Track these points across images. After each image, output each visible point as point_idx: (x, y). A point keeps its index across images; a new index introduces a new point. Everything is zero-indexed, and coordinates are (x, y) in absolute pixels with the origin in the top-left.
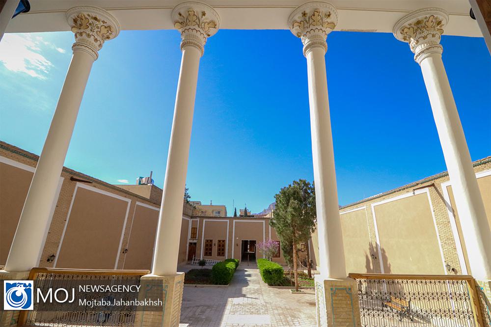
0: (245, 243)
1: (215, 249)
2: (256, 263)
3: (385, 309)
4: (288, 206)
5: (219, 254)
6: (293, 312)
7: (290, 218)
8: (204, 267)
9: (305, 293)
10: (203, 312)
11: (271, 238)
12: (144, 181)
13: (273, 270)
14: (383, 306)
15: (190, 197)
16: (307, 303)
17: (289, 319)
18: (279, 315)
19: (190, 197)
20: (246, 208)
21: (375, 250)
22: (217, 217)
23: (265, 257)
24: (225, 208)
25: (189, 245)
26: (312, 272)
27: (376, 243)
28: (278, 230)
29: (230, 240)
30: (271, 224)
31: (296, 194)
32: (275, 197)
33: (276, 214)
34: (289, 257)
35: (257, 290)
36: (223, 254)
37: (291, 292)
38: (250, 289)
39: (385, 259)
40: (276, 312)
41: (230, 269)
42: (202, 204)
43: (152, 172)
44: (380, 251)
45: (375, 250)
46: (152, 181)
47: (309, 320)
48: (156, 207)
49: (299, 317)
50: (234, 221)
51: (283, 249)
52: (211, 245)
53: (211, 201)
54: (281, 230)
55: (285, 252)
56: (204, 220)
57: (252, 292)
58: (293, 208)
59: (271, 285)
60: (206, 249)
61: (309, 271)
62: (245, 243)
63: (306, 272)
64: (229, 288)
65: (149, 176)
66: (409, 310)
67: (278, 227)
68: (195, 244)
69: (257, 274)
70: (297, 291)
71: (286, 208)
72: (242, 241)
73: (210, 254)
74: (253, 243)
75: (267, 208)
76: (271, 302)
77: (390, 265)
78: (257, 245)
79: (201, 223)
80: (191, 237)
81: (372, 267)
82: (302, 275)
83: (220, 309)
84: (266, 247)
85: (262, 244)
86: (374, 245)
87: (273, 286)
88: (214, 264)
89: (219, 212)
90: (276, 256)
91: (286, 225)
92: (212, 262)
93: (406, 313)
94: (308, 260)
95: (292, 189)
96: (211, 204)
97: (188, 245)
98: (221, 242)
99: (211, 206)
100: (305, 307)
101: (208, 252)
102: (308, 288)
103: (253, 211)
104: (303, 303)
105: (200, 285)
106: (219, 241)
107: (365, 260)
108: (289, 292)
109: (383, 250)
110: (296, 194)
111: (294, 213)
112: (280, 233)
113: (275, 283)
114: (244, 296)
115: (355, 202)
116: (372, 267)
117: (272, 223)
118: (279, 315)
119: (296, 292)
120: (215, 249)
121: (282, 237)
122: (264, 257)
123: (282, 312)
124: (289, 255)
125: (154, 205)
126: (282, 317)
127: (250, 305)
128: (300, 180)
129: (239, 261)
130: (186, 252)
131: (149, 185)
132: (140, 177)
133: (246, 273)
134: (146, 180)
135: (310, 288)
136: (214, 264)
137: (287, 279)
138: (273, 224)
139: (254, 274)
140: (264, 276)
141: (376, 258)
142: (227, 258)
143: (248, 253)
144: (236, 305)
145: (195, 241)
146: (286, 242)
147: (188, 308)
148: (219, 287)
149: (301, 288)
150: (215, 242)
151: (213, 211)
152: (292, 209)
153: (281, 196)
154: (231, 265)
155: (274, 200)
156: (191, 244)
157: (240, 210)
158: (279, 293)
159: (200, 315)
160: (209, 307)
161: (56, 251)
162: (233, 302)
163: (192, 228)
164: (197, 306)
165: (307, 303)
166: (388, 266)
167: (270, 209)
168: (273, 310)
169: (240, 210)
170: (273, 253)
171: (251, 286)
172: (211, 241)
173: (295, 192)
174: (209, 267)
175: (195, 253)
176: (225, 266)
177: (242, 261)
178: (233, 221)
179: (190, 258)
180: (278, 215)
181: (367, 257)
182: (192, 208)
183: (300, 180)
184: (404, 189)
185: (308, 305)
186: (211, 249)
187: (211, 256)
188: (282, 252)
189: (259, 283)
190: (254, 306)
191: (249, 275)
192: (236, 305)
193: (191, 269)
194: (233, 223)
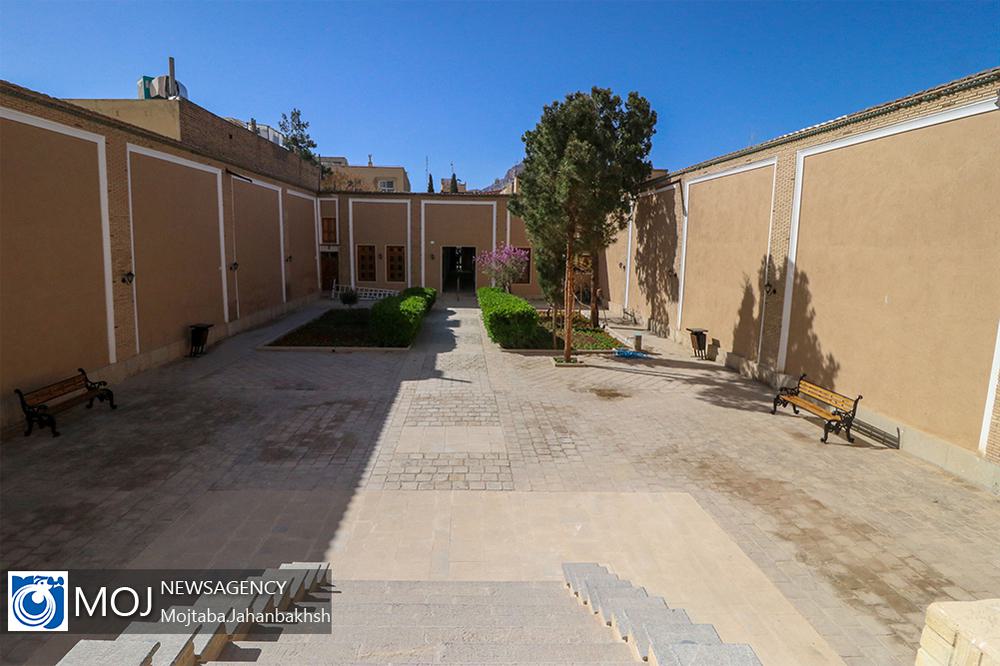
0: (450, 254)
1: (382, 267)
2: (475, 295)
3: (780, 408)
4: (561, 155)
5: (392, 277)
6: (560, 418)
7: (564, 191)
8: (354, 307)
9: (587, 366)
10: (340, 419)
11: (511, 243)
12: (156, 87)
13: (513, 316)
14: (777, 401)
15: (314, 146)
16: (592, 390)
17: (551, 436)
18: (527, 425)
19: (314, 146)
20: (454, 176)
21: (778, 276)
22: (370, 193)
23: (496, 285)
24: (405, 174)
25: (322, 259)
26: (601, 313)
27: (786, 259)
28: (531, 222)
29: (416, 247)
30: (513, 207)
31: (587, 122)
32: (524, 140)
33: (527, 182)
34: (554, 287)
35: (476, 358)
36: (402, 277)
37: (554, 363)
38: (459, 356)
39: (802, 296)
40: (519, 416)
41: (410, 313)
42: (350, 164)
43: (172, 60)
44: (790, 276)
45: (778, 276)
46: (178, 88)
47: (600, 438)
48: (201, 162)
49: (576, 430)
50: (423, 202)
51: (539, 269)
52: (372, 258)
53: (370, 156)
54: (540, 223)
55: (545, 276)
56: (351, 201)
57: (463, 364)
58: (575, 164)
59: (506, 346)
60: (391, 268)
61: (593, 313)
62: (450, 254)
63: (587, 314)
64: (413, 356)
65: (168, 75)
66: (848, 420)
67: (533, 216)
68: (335, 254)
69: (477, 320)
70: (568, 360)
71: (554, 164)
72: (444, 248)
73: (372, 277)
74: (469, 252)
75: (502, 177)
76: (508, 389)
77: (813, 312)
78: (477, 259)
79: (344, 206)
80: (324, 241)
81: (756, 314)
82: (578, 321)
83: (377, 411)
84: (499, 262)
85: (491, 256)
86: (778, 263)
87: (512, 348)
88: (382, 297)
89: (392, 184)
90: (521, 281)
91: (552, 209)
92: (370, 296)
93: (843, 425)
94: (595, 291)
95: (574, 107)
96: (370, 163)
97: (318, 257)
98: (396, 250)
99: (371, 167)
100: (587, 402)
101: (367, 272)
102: (591, 353)
103: (474, 182)
104: (582, 390)
105: (341, 348)
106: (391, 249)
107: (741, 296)
108: (550, 363)
109: (802, 279)
110: (587, 122)
111: (576, 177)
112: (537, 231)
113: (516, 343)
114: (439, 375)
115: (702, 161)
116: (756, 314)
117: (516, 204)
118: (527, 425)
119: (564, 363)
120: (382, 267)
121: (540, 241)
122: (494, 285)
123: (532, 416)
124: (554, 283)
125: (195, 155)
126: (534, 431)
127: (457, 398)
128: (595, 91)
129: (435, 293)
130: (316, 273)
131: (171, 98)
132: (145, 78)
133: (451, 318)
134: (160, 82)
135: (597, 353)
136: (382, 297)
137: (543, 331)
138: (517, 208)
139: (469, 322)
140: (491, 328)
141: (775, 292)
142: (409, 286)
143: (460, 273)
144: (424, 399)
145: (334, 249)
146: (550, 253)
147: (305, 408)
148: (387, 352)
149: (577, 354)
150: (381, 249)
151: (376, 181)
152: (573, 166)
153: (544, 131)
154: (413, 305)
155: (520, 155)
156: (324, 255)
157: (443, 180)
158: (526, 367)
159: (331, 428)
160: (356, 404)
161: (131, 267)
162: (411, 392)
163: (323, 219)
164: (328, 404)
165: (592, 390)
166: (808, 315)
167: (508, 177)
168: (512, 411)
169: (443, 180)
170: (514, 276)
171: (463, 349)
172: (372, 248)
173: (584, 116)
174: (365, 303)
175: (336, 274)
176: (398, 308)
177: (443, 290)
178: (420, 203)
179: (327, 286)
180: (532, 183)
181: (748, 292)
182: (318, 172)
183: (595, 91)
184: (939, 96)
185: (595, 395)
186: (372, 267)
187: (474, 249)
188: (535, 275)
189: (480, 341)
190: (466, 402)
191: (457, 323)
192: (424, 399)
193: (327, 310)
194: (420, 207)
